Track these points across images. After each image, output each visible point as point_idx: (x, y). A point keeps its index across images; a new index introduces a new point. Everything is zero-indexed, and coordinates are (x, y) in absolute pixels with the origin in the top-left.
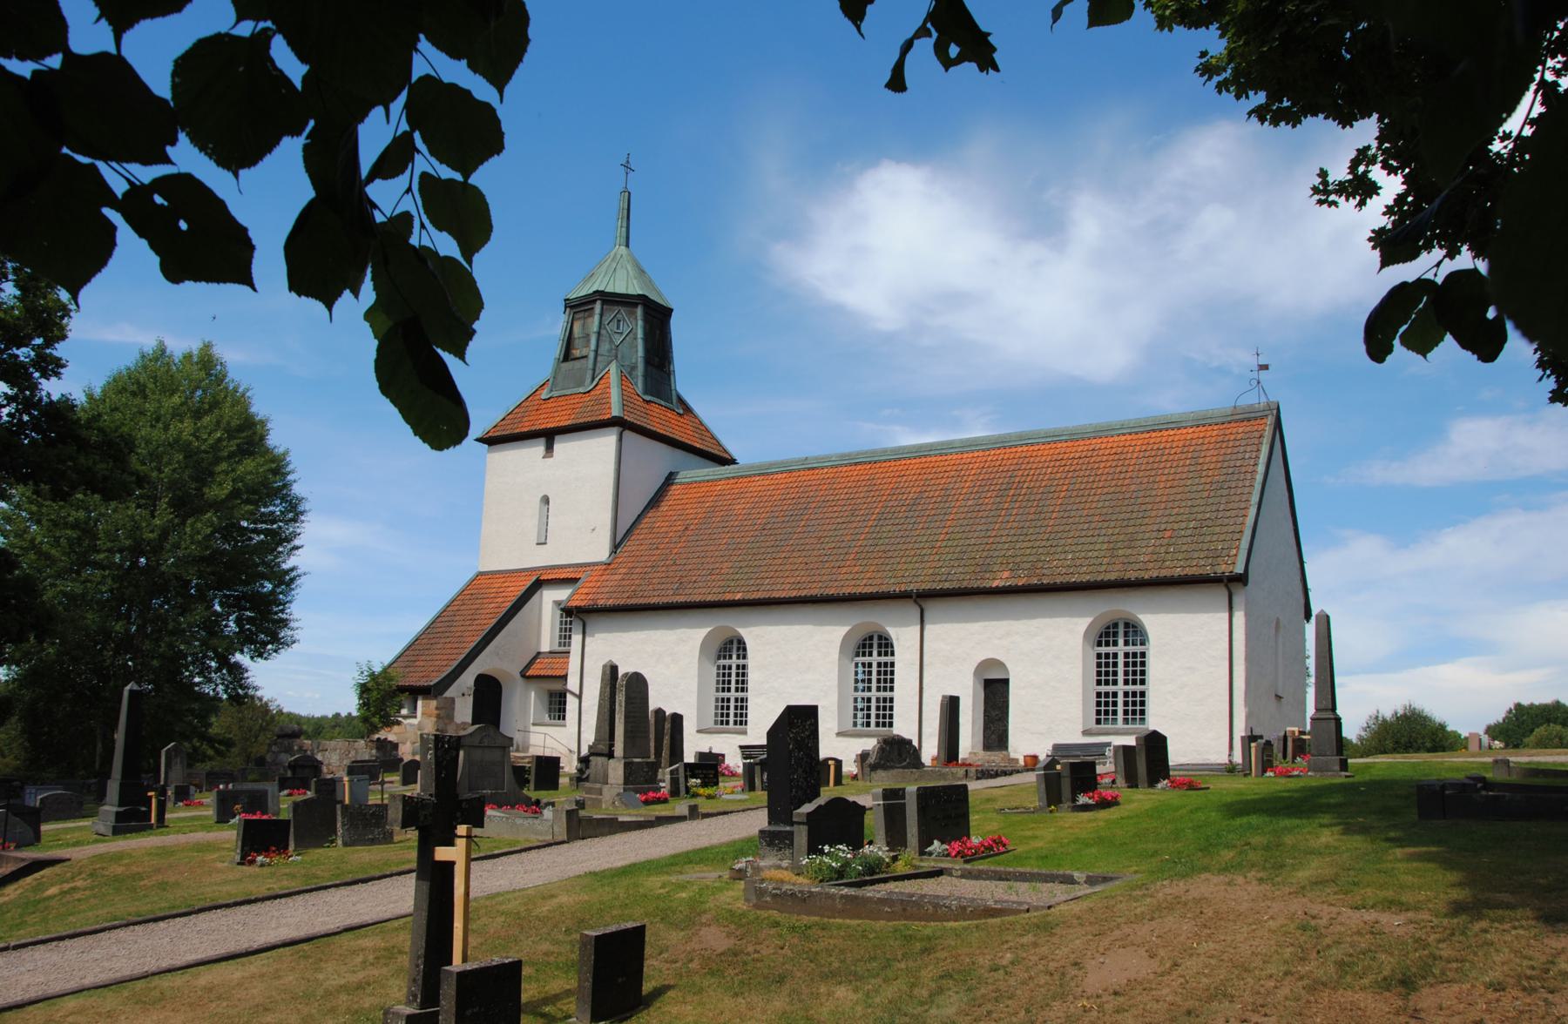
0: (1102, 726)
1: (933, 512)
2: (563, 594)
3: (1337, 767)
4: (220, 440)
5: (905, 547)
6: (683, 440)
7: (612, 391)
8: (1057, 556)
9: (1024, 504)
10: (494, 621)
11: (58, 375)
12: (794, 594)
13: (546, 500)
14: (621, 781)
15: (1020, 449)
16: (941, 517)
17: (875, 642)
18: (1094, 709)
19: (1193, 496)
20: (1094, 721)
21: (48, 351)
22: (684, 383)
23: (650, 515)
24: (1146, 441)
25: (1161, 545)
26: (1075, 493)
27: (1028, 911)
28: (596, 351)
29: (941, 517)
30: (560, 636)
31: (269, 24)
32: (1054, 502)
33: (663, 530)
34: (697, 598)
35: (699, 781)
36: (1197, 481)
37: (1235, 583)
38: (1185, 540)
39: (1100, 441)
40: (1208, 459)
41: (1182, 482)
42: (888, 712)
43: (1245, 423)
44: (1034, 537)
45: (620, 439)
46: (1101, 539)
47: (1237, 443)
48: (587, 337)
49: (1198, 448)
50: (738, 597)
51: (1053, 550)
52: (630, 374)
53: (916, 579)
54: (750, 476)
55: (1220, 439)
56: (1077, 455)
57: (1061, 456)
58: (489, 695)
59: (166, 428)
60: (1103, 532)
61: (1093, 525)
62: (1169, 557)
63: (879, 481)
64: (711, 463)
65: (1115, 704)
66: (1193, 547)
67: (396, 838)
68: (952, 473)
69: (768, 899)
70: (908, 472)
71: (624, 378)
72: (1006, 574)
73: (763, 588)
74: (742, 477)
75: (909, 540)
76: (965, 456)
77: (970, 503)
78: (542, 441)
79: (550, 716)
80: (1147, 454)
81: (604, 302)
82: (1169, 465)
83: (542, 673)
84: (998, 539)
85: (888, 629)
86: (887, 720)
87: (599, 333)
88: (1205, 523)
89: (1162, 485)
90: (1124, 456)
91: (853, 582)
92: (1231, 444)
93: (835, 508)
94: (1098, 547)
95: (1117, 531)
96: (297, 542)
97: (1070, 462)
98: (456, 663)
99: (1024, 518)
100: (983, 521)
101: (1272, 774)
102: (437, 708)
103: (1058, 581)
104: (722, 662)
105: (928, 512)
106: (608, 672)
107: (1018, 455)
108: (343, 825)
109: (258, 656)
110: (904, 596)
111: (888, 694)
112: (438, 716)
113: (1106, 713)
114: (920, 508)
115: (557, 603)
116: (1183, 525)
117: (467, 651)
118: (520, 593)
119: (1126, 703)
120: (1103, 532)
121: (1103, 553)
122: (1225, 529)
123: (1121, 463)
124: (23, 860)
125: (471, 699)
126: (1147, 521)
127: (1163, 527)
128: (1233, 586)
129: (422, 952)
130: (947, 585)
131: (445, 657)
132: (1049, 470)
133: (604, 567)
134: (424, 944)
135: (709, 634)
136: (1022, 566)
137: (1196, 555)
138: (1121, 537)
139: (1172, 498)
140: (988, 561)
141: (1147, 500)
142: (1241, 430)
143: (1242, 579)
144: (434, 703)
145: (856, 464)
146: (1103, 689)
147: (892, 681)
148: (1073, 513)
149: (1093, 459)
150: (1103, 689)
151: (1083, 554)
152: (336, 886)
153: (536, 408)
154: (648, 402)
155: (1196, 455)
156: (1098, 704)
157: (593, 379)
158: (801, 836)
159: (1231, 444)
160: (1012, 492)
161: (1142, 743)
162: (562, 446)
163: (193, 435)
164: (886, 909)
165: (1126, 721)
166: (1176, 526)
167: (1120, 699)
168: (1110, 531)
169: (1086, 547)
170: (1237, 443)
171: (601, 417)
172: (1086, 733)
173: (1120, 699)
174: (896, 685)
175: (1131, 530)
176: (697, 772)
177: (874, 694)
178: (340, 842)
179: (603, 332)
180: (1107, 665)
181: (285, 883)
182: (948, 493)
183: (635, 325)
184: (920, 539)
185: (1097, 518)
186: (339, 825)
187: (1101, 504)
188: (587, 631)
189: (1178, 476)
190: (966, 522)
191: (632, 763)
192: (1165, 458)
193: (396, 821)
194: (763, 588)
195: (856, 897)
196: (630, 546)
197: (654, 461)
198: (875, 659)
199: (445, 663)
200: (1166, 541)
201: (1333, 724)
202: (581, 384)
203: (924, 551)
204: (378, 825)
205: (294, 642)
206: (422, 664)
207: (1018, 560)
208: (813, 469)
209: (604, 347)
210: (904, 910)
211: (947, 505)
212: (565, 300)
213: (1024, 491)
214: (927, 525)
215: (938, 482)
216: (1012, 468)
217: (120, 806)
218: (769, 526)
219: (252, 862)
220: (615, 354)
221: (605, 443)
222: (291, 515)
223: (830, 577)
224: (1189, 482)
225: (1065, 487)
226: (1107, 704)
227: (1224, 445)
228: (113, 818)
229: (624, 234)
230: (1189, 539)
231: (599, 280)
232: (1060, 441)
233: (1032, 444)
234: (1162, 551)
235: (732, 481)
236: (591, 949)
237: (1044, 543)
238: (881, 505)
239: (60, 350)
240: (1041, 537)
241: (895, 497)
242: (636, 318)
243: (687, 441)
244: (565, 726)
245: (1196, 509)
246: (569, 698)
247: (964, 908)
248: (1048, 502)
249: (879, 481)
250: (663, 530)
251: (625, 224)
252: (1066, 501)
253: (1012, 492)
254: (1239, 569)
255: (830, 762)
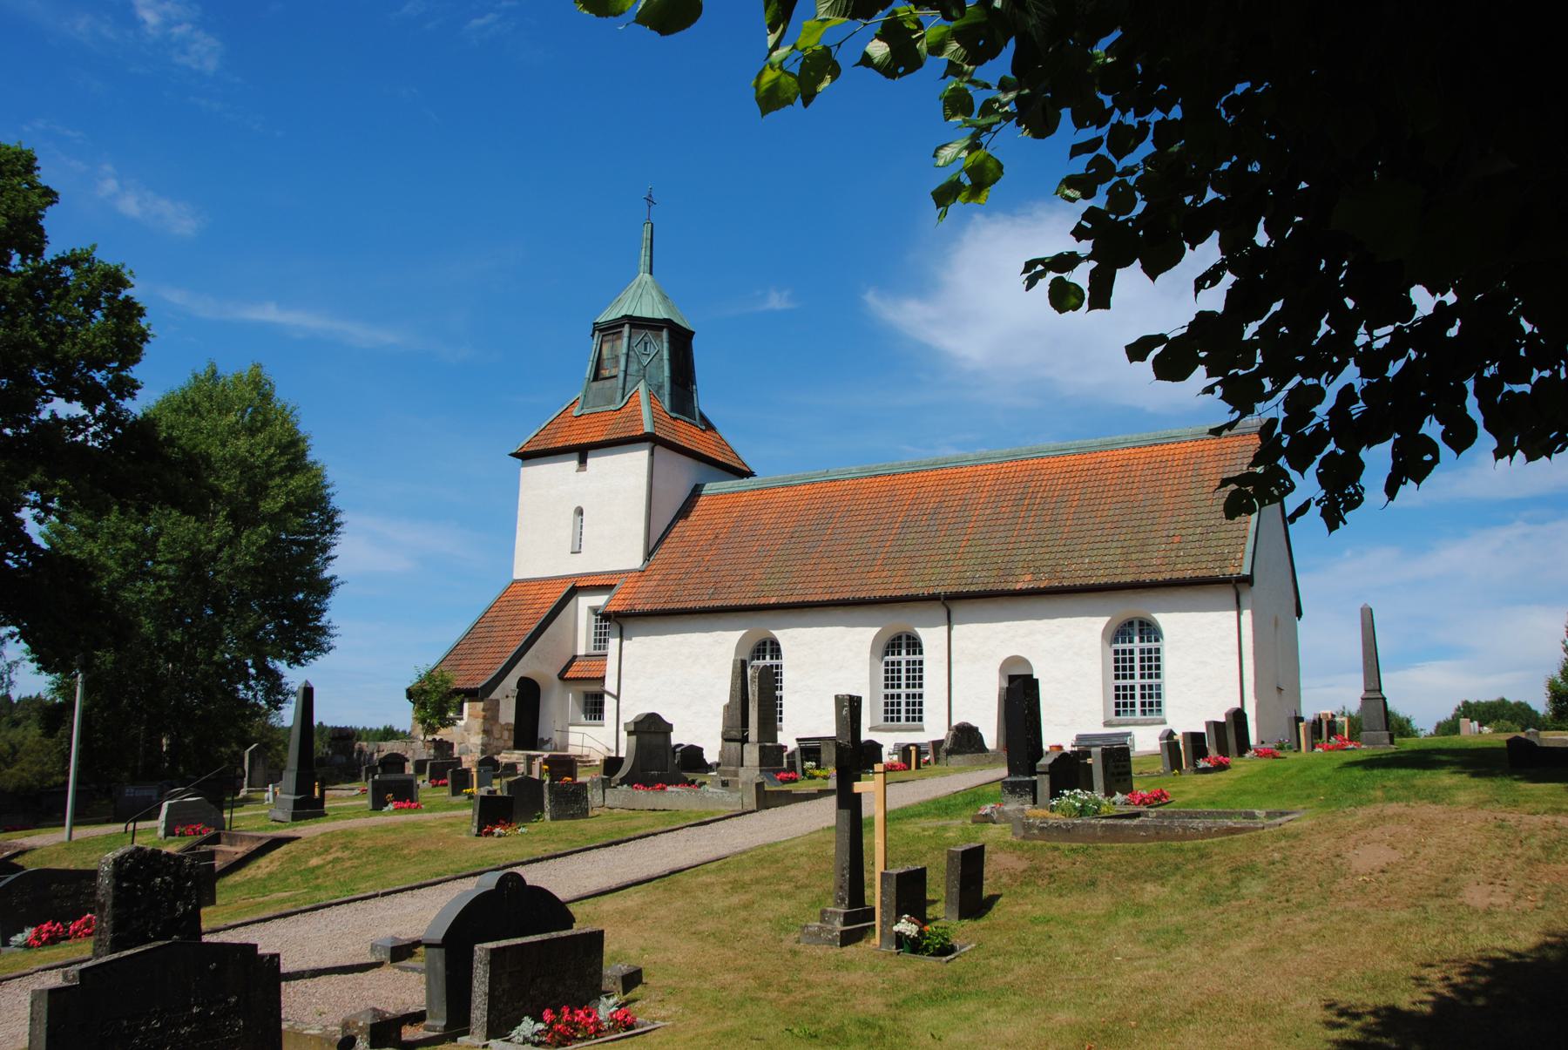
0: (1121, 717)
1: (953, 521)
2: (600, 600)
3: (1387, 741)
4: (272, 456)
5: (930, 553)
6: (707, 454)
7: (642, 408)
8: (1074, 561)
9: (1039, 512)
10: (534, 627)
11: (132, 395)
12: (827, 597)
13: (580, 512)
14: (757, 762)
15: (1031, 462)
16: (961, 525)
17: (768, 648)
18: (1113, 701)
19: (1197, 504)
20: (1114, 713)
21: (124, 373)
22: (705, 401)
23: (679, 524)
24: (1149, 454)
25: (1172, 550)
26: (1086, 502)
27: (1263, 828)
28: (626, 371)
29: (961, 525)
30: (595, 640)
31: (1470, 384)
32: (1067, 510)
33: (693, 538)
34: (733, 603)
35: (814, 764)
36: (1200, 490)
37: (1242, 584)
38: (1193, 545)
39: (1106, 454)
40: (1208, 471)
41: (1186, 492)
42: (917, 708)
43: (1240, 438)
44: (1051, 543)
45: (652, 454)
46: (1114, 544)
47: (1234, 456)
48: (616, 358)
49: (1199, 461)
50: (773, 600)
51: (1070, 555)
52: (657, 392)
53: (942, 583)
54: (774, 488)
55: (1218, 452)
56: (1086, 467)
57: (1070, 469)
58: (529, 694)
59: (224, 445)
60: (1116, 537)
61: (1106, 532)
62: (1179, 560)
63: (899, 492)
64: (732, 476)
65: (1133, 696)
66: (1202, 550)
67: (590, 814)
68: (969, 485)
69: (1036, 831)
70: (926, 484)
71: (654, 395)
72: (1028, 577)
73: (797, 592)
74: (766, 488)
75: (932, 546)
76: (980, 468)
77: (988, 512)
78: (576, 455)
79: (586, 717)
80: (1151, 466)
81: (632, 326)
82: (1172, 476)
83: (580, 675)
84: (1017, 545)
85: (916, 629)
86: (917, 715)
87: (628, 355)
88: (1210, 530)
89: (1167, 495)
90: (1130, 468)
91: (883, 586)
92: (1229, 457)
93: (859, 518)
94: (1112, 551)
95: (1129, 537)
96: (332, 552)
97: (1079, 474)
98: (500, 667)
99: (1040, 525)
100: (1002, 528)
101: (1320, 750)
102: (484, 710)
103: (1078, 583)
104: (890, 658)
105: (948, 521)
106: (739, 666)
107: (1030, 467)
108: (550, 801)
109: (294, 663)
110: (933, 598)
111: (917, 691)
112: (485, 718)
113: (1125, 705)
114: (940, 516)
115: (594, 610)
116: (1191, 531)
117: (510, 655)
118: (558, 600)
119: (1143, 696)
120: (1116, 537)
121: (1118, 557)
122: (1229, 535)
123: (1127, 474)
124: (260, 838)
125: (513, 701)
126: (1155, 527)
127: (1172, 533)
128: (1240, 587)
129: (847, 864)
130: (973, 588)
131: (489, 661)
132: (1061, 481)
133: (639, 574)
134: (848, 858)
135: (1109, 622)
136: (1043, 569)
137: (1204, 558)
138: (1134, 543)
139: (1178, 506)
140: (1010, 565)
141: (1155, 508)
142: (1237, 444)
143: (1248, 580)
144: (480, 705)
145: (876, 476)
146: (1121, 682)
147: (921, 678)
148: (1086, 521)
149: (1101, 471)
150: (1121, 682)
151: (1099, 558)
152: (597, 847)
153: (568, 424)
154: (675, 419)
155: (1196, 467)
156: (1117, 697)
157: (623, 398)
158: (1044, 784)
159: (1229, 457)
160: (1026, 502)
161: (1231, 718)
162: (595, 462)
163: (248, 451)
164: (1142, 833)
165: (1144, 712)
166: (1183, 532)
167: (1138, 692)
168: (1122, 537)
169: (1101, 552)
170: (1234, 456)
171: (633, 434)
172: (1107, 724)
173: (1138, 692)
174: (925, 681)
175: (1141, 535)
176: (811, 755)
177: (903, 691)
178: (547, 817)
179: (631, 353)
180: (1124, 660)
181: (561, 846)
182: (966, 502)
183: (662, 346)
184: (943, 545)
185: (1109, 525)
186: (546, 801)
187: (1111, 513)
188: (624, 634)
189: (1181, 487)
190: (985, 529)
191: (765, 746)
192: (1168, 470)
193: (830, 762)
194: (797, 592)
195: (1116, 825)
196: (662, 553)
197: (681, 474)
198: (1137, 645)
199: (489, 666)
200: (1175, 546)
201: (1381, 702)
202: (611, 401)
203: (948, 557)
204: (576, 802)
205: (330, 648)
206: (465, 667)
207: (1038, 564)
208: (835, 480)
209: (633, 367)
210: (1158, 833)
211: (966, 513)
212: (595, 324)
213: (1038, 501)
214: (948, 533)
215: (956, 492)
216: (1025, 479)
217: (296, 794)
218: (797, 534)
219: (490, 833)
220: (643, 374)
221: (637, 461)
222: (328, 527)
223: (860, 582)
224: (1192, 492)
225: (1077, 497)
226: (1125, 697)
227: (1222, 458)
228: (291, 806)
229: (648, 263)
230: (1197, 544)
231: (627, 305)
232: (1069, 455)
233: (1042, 458)
234: (1173, 554)
235: (757, 492)
236: (958, 861)
237: (1061, 549)
238: (903, 514)
239: (135, 372)
240: (1058, 542)
241: (916, 507)
242: (662, 341)
243: (710, 455)
244: (603, 725)
245: (1201, 517)
246: (607, 698)
247: (1210, 829)
248: (1062, 511)
249: (899, 492)
250: (693, 538)
251: (648, 253)
252: (1079, 509)
253: (1026, 502)
254: (1246, 571)
255: (911, 748)
